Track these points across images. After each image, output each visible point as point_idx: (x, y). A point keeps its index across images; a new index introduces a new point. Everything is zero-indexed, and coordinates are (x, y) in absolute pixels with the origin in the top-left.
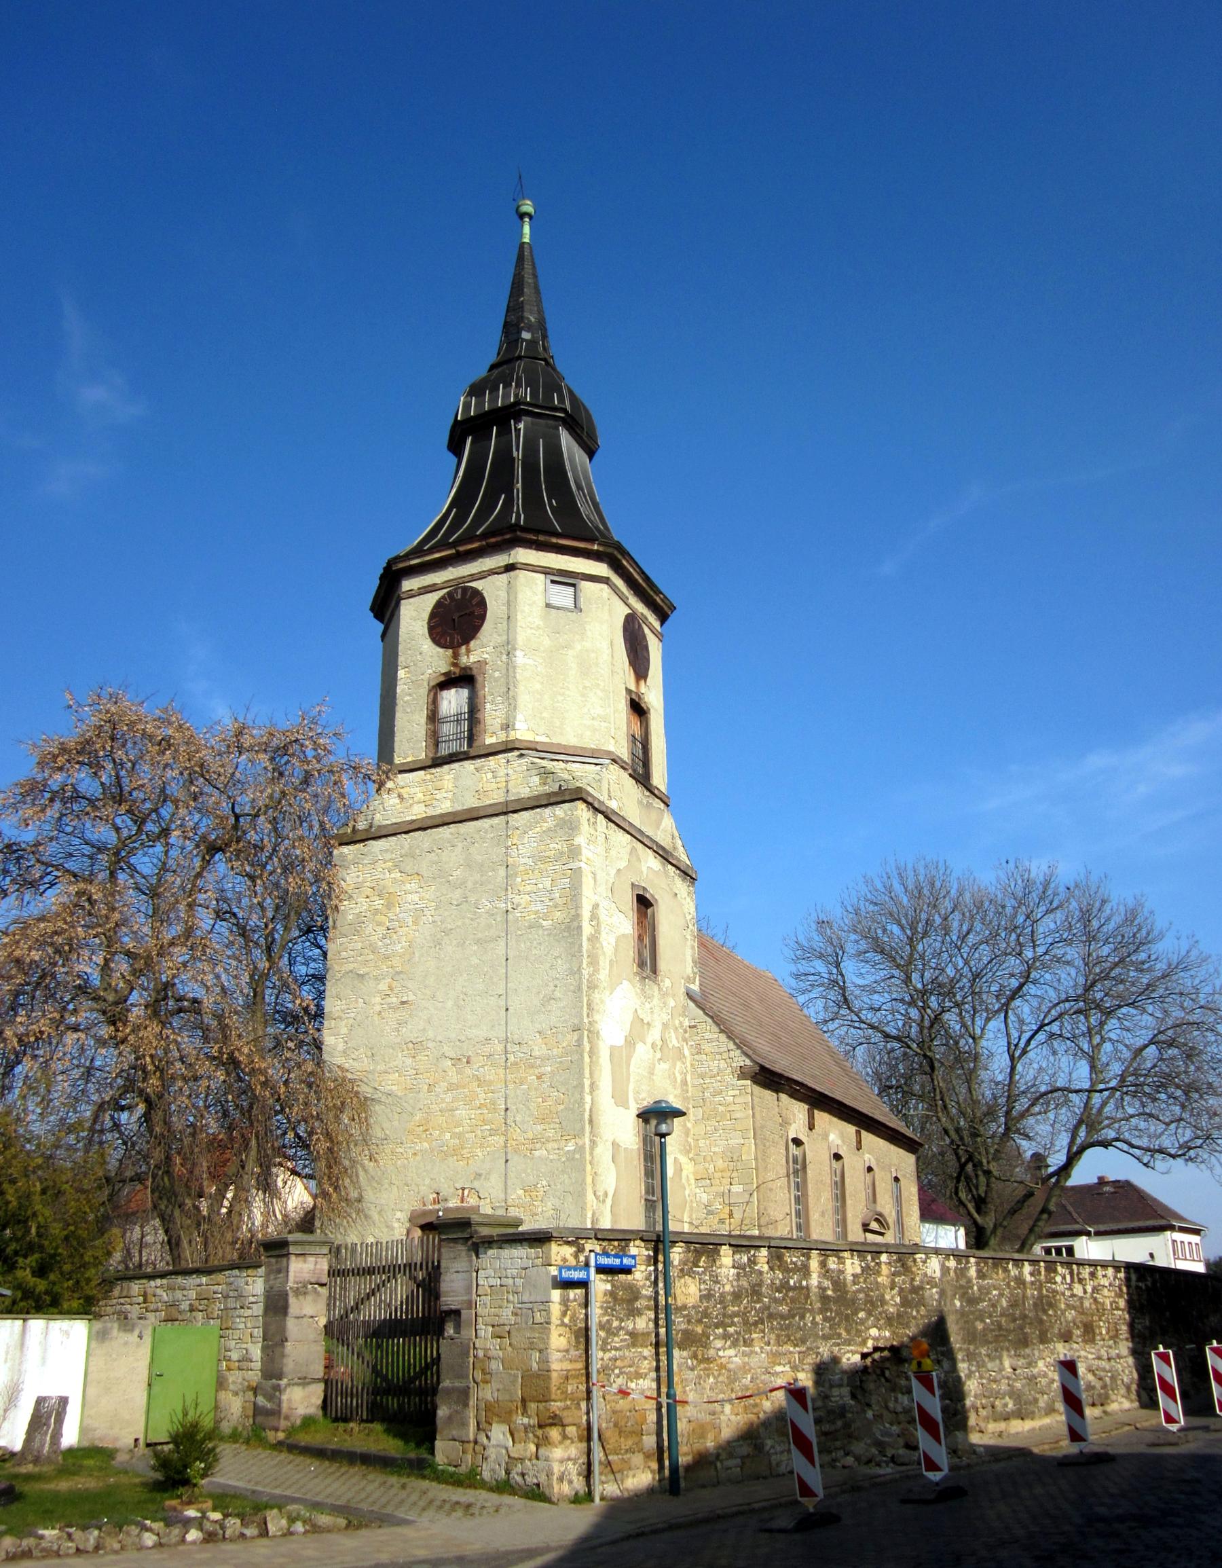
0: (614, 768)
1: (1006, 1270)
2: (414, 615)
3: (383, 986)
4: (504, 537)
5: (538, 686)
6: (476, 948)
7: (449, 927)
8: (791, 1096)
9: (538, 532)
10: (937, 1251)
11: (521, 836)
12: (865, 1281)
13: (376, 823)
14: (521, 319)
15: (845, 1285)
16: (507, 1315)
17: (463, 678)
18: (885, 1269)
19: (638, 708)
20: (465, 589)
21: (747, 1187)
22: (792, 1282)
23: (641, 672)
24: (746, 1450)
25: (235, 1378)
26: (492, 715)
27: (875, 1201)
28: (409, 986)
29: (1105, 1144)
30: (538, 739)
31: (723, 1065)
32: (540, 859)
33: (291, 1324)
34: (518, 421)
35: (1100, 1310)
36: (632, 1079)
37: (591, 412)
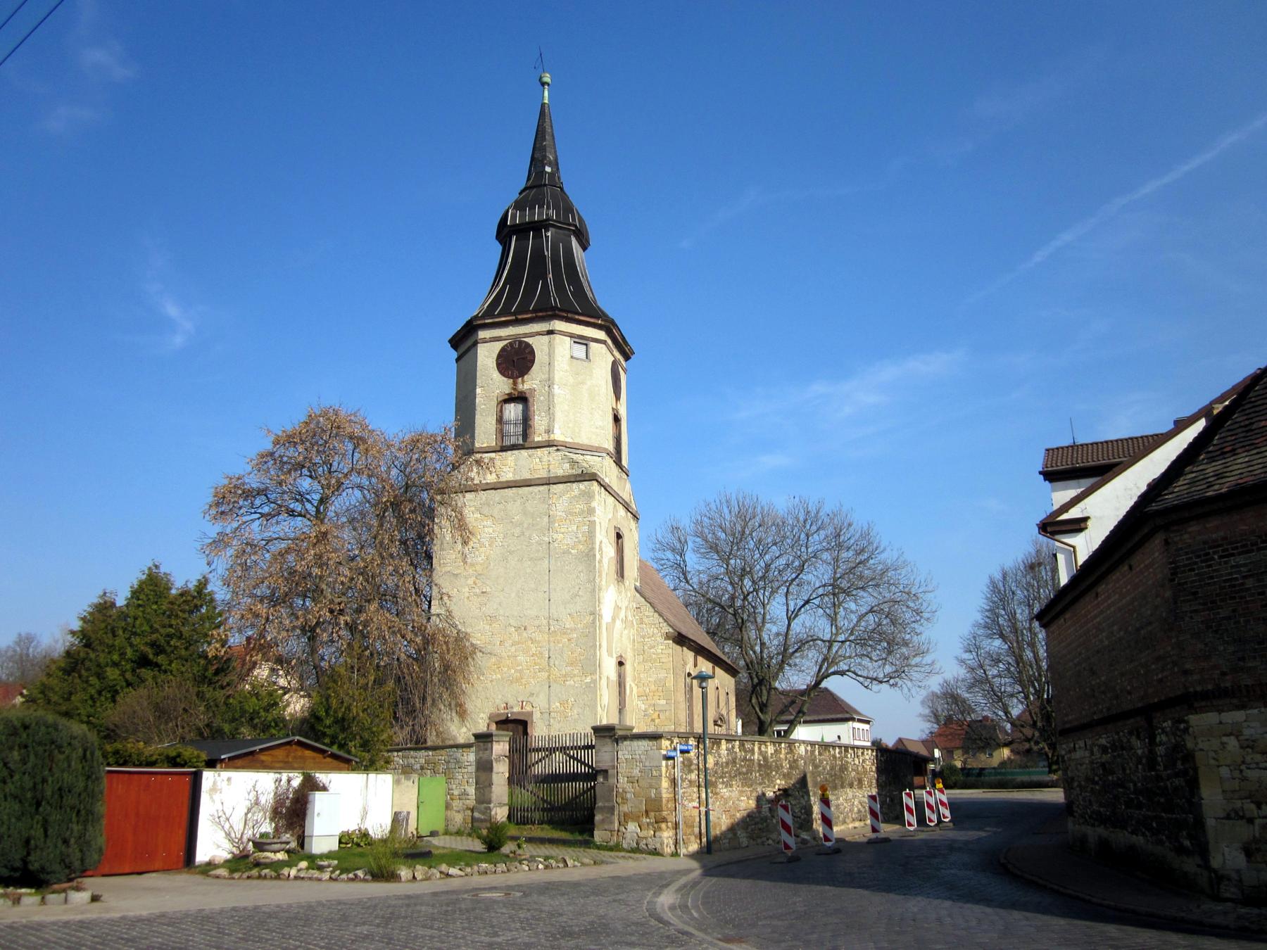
2: (487, 355)
3: (470, 582)
4: (546, 312)
9: (568, 312)
10: (804, 742)
14: (545, 157)
16: (636, 772)
17: (521, 398)
20: (521, 342)
23: (618, 397)
24: (730, 835)
25: (456, 804)
26: (539, 422)
29: (842, 673)
32: (569, 513)
33: (494, 776)
35: (865, 772)
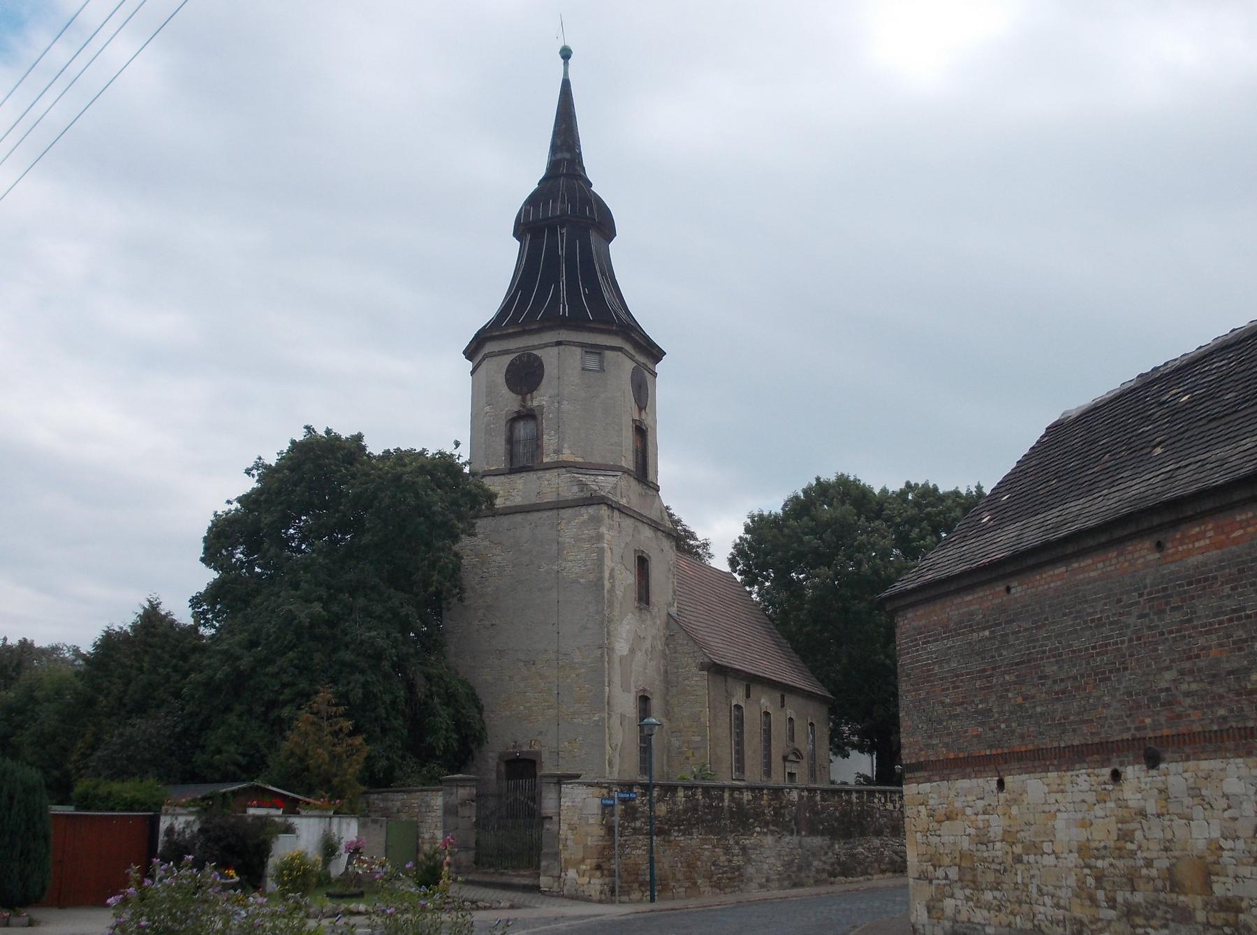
4: (554, 321)
17: (528, 414)
20: (530, 355)
31: (690, 661)
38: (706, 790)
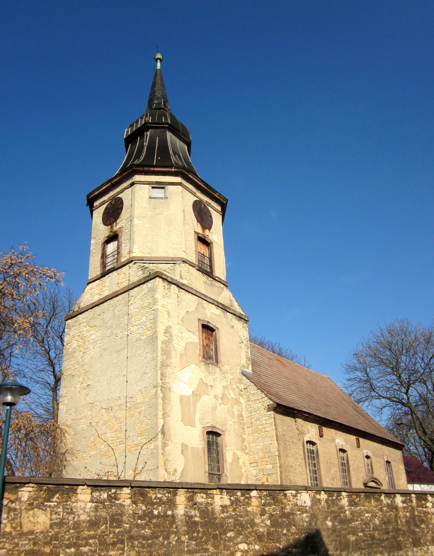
0: (186, 267)
1: (378, 500)
3: (81, 379)
5: (145, 232)
6: (115, 355)
7: (106, 347)
8: (305, 420)
11: (134, 299)
12: (234, 510)
13: (81, 307)
15: (213, 512)
18: (255, 502)
19: (203, 241)
20: (116, 199)
21: (274, 466)
22: (156, 512)
27: (372, 472)
28: (91, 377)
30: (144, 255)
31: (260, 405)
34: (147, 131)
36: (197, 412)
37: (185, 124)
38: (140, 490)
